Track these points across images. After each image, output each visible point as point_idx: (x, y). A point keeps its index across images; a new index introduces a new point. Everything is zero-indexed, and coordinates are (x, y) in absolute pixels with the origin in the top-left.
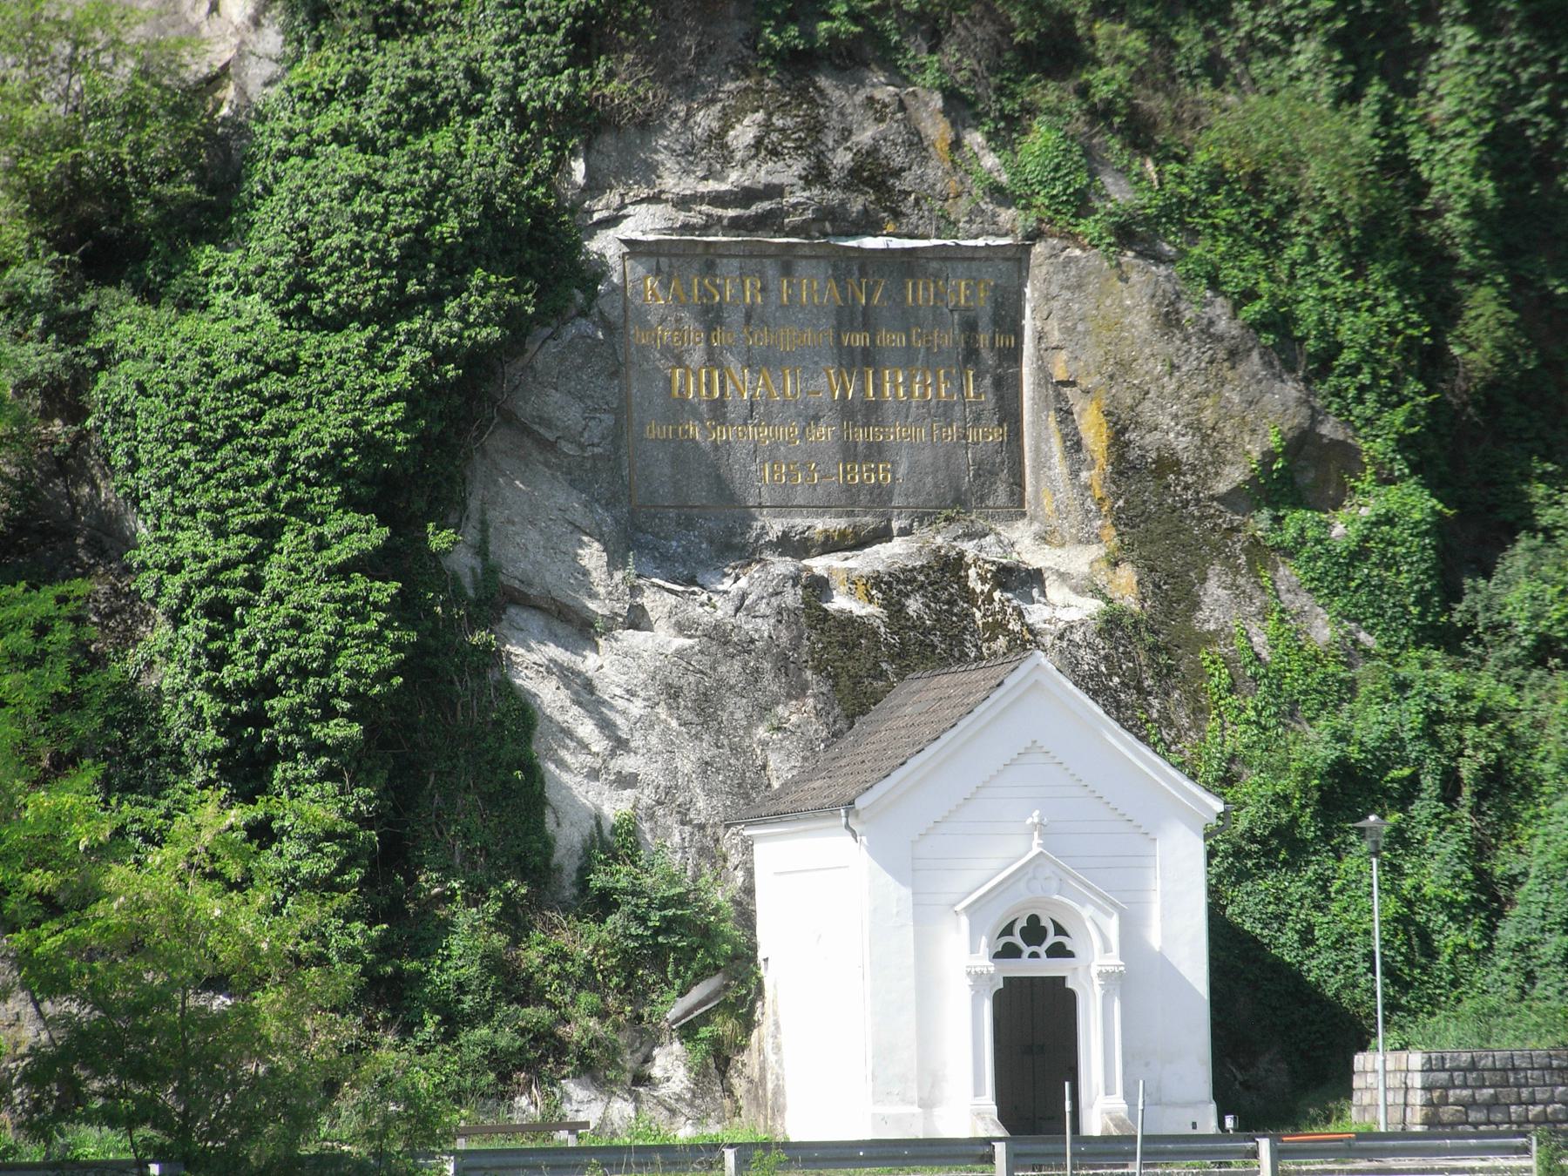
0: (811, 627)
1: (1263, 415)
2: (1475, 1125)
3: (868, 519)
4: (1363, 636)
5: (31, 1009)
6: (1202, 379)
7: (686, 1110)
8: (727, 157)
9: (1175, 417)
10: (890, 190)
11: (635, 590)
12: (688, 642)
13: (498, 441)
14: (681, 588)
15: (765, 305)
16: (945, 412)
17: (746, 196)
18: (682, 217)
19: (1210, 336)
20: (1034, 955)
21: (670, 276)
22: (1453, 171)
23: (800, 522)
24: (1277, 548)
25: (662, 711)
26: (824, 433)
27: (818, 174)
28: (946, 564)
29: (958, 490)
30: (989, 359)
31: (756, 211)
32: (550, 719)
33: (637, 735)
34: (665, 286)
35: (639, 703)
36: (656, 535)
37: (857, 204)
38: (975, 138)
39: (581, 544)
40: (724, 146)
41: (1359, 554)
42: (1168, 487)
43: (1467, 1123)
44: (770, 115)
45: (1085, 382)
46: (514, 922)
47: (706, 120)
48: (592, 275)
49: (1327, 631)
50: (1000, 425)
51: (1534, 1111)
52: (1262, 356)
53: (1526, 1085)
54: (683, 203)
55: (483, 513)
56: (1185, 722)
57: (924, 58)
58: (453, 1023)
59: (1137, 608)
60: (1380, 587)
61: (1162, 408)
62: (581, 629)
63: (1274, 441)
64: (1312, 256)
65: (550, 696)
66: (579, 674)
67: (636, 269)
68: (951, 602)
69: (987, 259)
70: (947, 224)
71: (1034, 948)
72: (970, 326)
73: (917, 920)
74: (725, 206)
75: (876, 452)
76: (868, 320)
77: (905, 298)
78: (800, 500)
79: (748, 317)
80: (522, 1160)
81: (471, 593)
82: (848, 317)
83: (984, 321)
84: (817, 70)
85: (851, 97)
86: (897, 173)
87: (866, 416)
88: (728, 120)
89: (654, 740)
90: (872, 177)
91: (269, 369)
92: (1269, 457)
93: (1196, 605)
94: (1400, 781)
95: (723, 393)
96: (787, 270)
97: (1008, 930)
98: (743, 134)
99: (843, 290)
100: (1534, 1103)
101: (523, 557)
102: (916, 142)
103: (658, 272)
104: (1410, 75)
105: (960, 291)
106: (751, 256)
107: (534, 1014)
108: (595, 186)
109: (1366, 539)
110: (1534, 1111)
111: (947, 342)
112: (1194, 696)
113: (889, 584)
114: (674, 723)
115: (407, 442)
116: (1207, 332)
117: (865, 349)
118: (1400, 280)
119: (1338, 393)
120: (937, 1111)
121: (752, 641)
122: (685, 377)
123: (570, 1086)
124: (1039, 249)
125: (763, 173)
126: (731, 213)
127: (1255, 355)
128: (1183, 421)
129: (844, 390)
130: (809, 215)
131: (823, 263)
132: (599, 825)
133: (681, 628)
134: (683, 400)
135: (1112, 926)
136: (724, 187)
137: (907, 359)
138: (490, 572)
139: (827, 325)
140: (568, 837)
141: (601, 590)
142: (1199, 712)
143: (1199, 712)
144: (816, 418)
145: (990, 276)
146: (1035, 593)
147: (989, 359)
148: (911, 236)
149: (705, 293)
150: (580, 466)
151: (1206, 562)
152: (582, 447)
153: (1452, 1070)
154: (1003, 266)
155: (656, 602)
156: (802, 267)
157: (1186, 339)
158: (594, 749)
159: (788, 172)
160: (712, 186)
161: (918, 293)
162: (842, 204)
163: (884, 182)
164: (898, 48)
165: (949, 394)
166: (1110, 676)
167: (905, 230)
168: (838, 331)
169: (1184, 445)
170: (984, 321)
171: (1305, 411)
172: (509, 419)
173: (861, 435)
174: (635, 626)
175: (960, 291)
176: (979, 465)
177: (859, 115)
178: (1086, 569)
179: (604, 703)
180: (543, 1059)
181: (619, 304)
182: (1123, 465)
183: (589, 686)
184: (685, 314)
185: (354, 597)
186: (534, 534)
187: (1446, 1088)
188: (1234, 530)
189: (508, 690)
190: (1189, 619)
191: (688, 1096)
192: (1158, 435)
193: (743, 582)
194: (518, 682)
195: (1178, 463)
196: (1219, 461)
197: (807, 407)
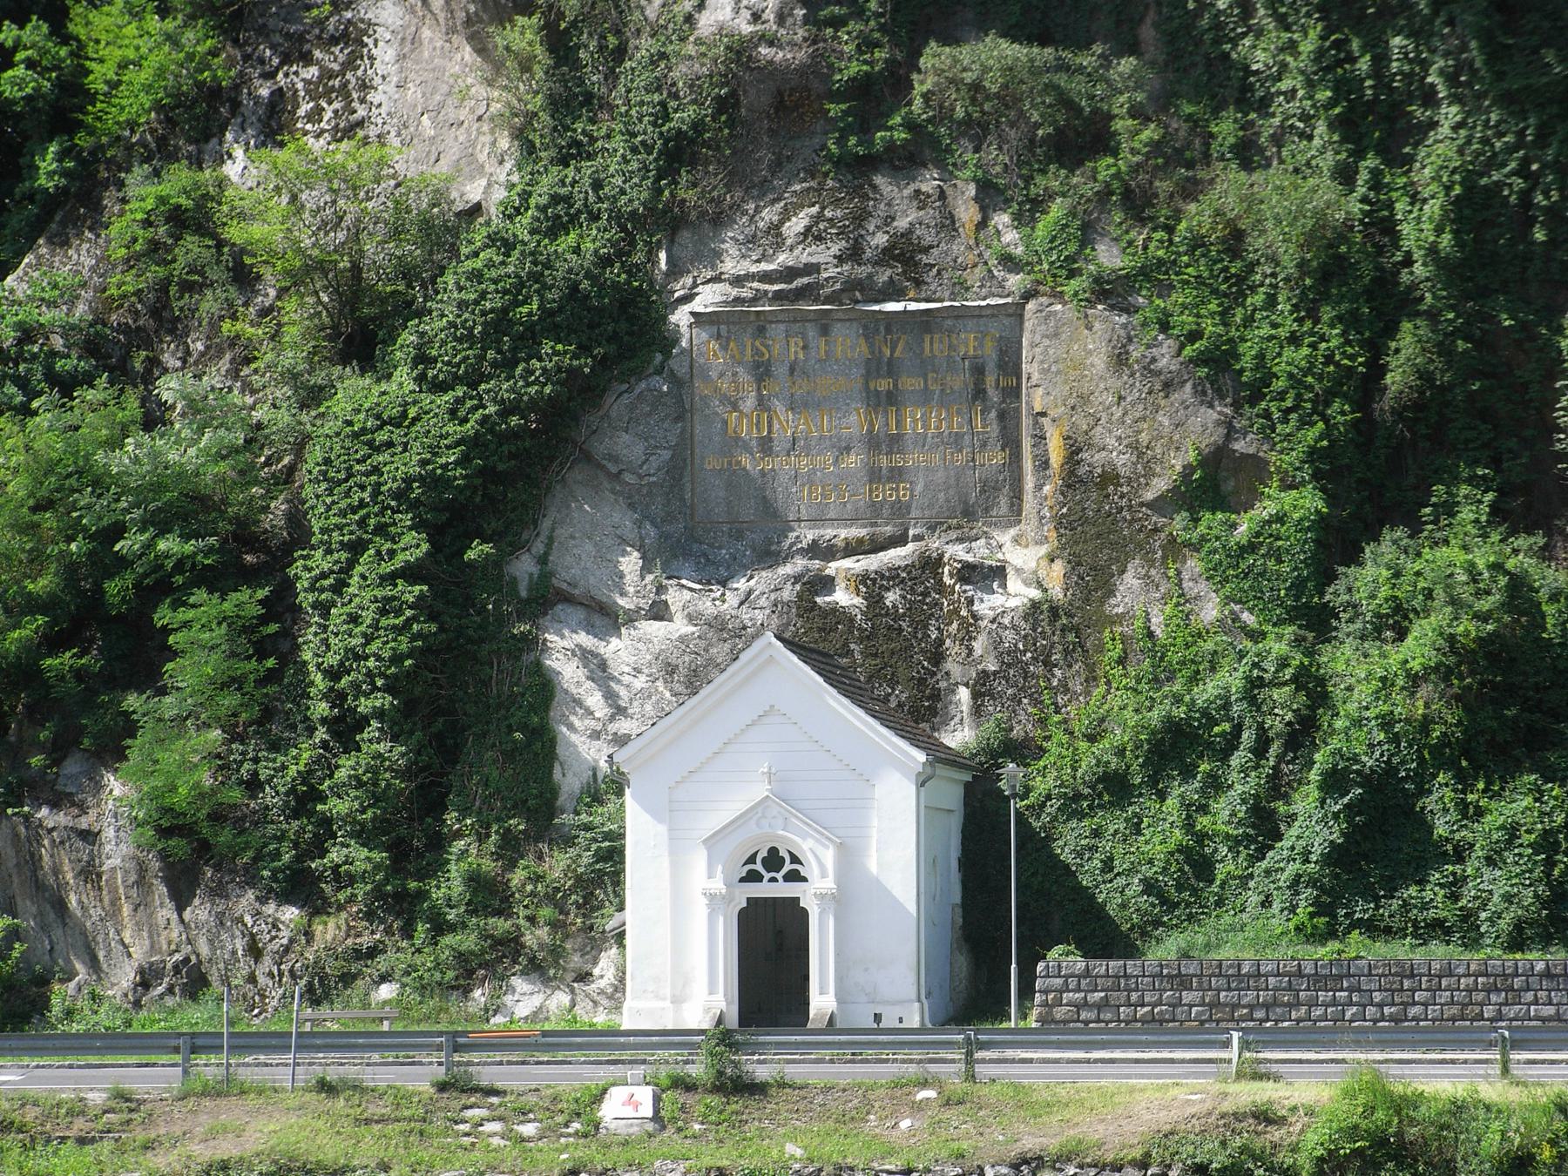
0: (799, 616)
1: (1190, 430)
2: (1086, 1023)
3: (889, 528)
4: (1245, 616)
5: (175, 916)
6: (1141, 407)
7: (605, 1002)
8: (779, 244)
9: (1119, 439)
10: (916, 264)
11: (661, 589)
12: (692, 629)
13: (577, 474)
14: (698, 587)
15: (806, 360)
16: (956, 441)
17: (789, 273)
18: (735, 292)
19: (1150, 371)
20: (773, 880)
21: (728, 339)
22: (1421, 227)
23: (829, 532)
24: (1188, 544)
25: (660, 684)
26: (854, 461)
27: (853, 254)
28: (927, 563)
29: (966, 503)
30: (994, 395)
31: (798, 286)
32: (566, 692)
33: (635, 704)
34: (725, 348)
35: (643, 678)
36: (711, 545)
37: (883, 276)
38: (1002, 219)
39: (624, 553)
40: (779, 235)
41: (1251, 548)
42: (1107, 496)
43: (1078, 1021)
44: (823, 208)
45: (1052, 413)
46: (510, 850)
47: (769, 215)
48: (668, 342)
49: (1214, 613)
50: (1003, 450)
51: (1142, 1011)
52: (1194, 386)
53: (1137, 990)
54: (738, 281)
55: (553, 530)
56: (1079, 689)
57: (968, 156)
58: (440, 927)
59: (1061, 596)
60: (1262, 574)
61: (1110, 432)
62: (606, 618)
63: (1192, 456)
64: (1271, 301)
65: (568, 671)
66: (597, 655)
67: (701, 335)
68: (925, 594)
69: (993, 315)
70: (961, 288)
71: (773, 874)
72: (979, 371)
73: (673, 852)
74: (771, 283)
75: (897, 474)
76: (892, 369)
77: (923, 350)
78: (832, 515)
79: (792, 370)
80: (262, 1042)
81: (524, 594)
82: (875, 367)
83: (991, 367)
84: (876, 170)
85: (900, 190)
86: (926, 250)
87: (890, 446)
88: (785, 216)
89: (648, 707)
90: (902, 254)
91: (384, 423)
92: (1188, 469)
93: (1111, 593)
94: (1223, 734)
95: (770, 432)
96: (825, 331)
97: (752, 859)
98: (797, 224)
99: (871, 346)
100: (1143, 1005)
101: (575, 565)
102: (949, 224)
103: (719, 337)
104: (1407, 150)
105: (968, 342)
106: (795, 321)
107: (500, 925)
108: (675, 271)
109: (1258, 534)
110: (1142, 1011)
111: (957, 386)
112: (1091, 668)
113: (873, 580)
114: (668, 694)
115: (463, 477)
116: (1149, 370)
117: (889, 392)
118: (1349, 321)
119: (1267, 414)
120: (685, 1006)
121: (745, 628)
122: (739, 419)
123: (517, 981)
124: (1031, 306)
125: (803, 256)
126: (776, 287)
127: (1189, 386)
128: (1125, 442)
129: (871, 425)
130: (838, 286)
131: (855, 324)
132: (595, 775)
133: (691, 618)
134: (738, 439)
135: (829, 856)
136: (772, 267)
137: (925, 398)
138: (546, 576)
139: (857, 373)
140: (569, 783)
141: (631, 590)
142: (1091, 680)
143: (1091, 680)
144: (848, 449)
145: (995, 329)
146: (995, 585)
147: (994, 395)
148: (928, 300)
149: (757, 352)
150: (639, 491)
151: (1129, 557)
152: (641, 477)
153: (1067, 977)
154: (1006, 321)
155: (676, 598)
156: (838, 330)
157: (1132, 375)
158: (597, 715)
159: (823, 254)
160: (765, 266)
161: (934, 346)
162: (870, 276)
163: (912, 258)
164: (949, 150)
165: (960, 426)
166: (1025, 652)
167: (923, 295)
168: (868, 376)
169: (1122, 461)
170: (991, 367)
171: (1222, 431)
172: (587, 457)
173: (884, 461)
174: (658, 617)
175: (968, 342)
176: (985, 483)
177: (900, 205)
178: (1034, 564)
179: (613, 678)
180: (499, 960)
181: (686, 364)
182: (1073, 479)
183: (603, 665)
184: (740, 370)
185: (394, 598)
186: (589, 547)
187: (1061, 992)
188: (1156, 530)
189: (538, 669)
190: (1103, 604)
191: (610, 990)
192: (1104, 454)
193: (752, 582)
194: (548, 662)
195: (1118, 476)
196: (1150, 474)
197: (840, 440)
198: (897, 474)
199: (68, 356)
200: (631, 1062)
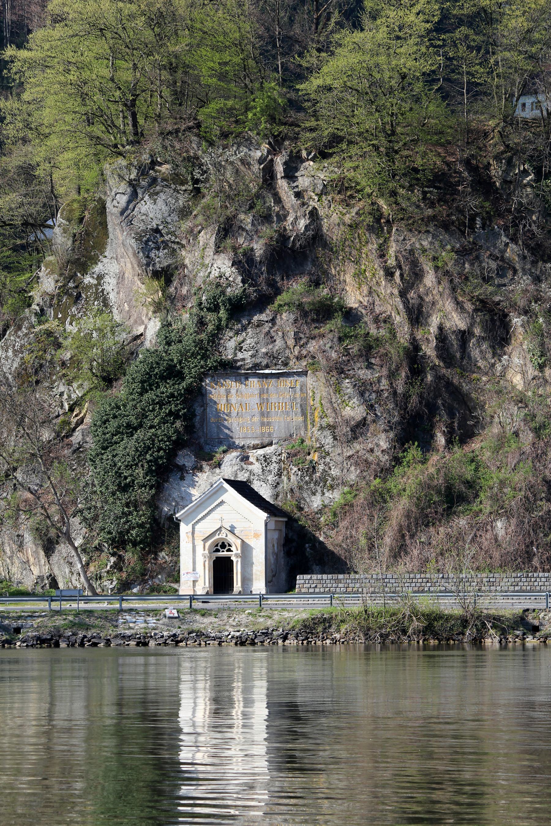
97: (217, 545)
110: (327, 589)
198: (269, 424)
199: (122, 440)
200: (277, 376)
